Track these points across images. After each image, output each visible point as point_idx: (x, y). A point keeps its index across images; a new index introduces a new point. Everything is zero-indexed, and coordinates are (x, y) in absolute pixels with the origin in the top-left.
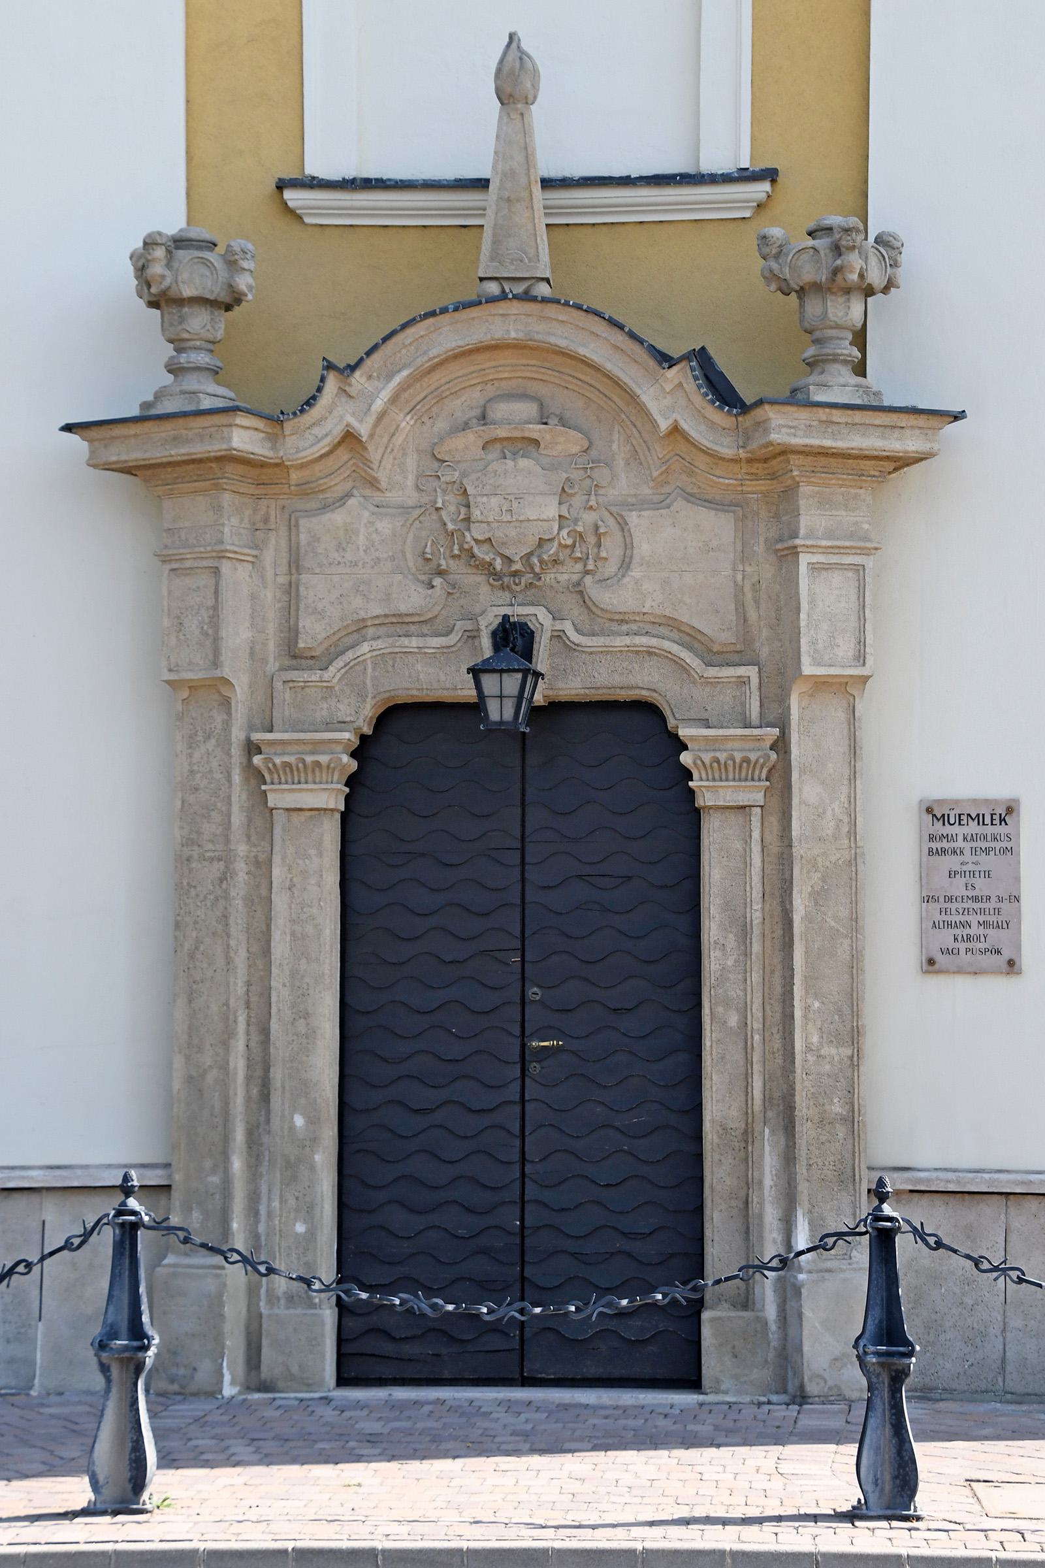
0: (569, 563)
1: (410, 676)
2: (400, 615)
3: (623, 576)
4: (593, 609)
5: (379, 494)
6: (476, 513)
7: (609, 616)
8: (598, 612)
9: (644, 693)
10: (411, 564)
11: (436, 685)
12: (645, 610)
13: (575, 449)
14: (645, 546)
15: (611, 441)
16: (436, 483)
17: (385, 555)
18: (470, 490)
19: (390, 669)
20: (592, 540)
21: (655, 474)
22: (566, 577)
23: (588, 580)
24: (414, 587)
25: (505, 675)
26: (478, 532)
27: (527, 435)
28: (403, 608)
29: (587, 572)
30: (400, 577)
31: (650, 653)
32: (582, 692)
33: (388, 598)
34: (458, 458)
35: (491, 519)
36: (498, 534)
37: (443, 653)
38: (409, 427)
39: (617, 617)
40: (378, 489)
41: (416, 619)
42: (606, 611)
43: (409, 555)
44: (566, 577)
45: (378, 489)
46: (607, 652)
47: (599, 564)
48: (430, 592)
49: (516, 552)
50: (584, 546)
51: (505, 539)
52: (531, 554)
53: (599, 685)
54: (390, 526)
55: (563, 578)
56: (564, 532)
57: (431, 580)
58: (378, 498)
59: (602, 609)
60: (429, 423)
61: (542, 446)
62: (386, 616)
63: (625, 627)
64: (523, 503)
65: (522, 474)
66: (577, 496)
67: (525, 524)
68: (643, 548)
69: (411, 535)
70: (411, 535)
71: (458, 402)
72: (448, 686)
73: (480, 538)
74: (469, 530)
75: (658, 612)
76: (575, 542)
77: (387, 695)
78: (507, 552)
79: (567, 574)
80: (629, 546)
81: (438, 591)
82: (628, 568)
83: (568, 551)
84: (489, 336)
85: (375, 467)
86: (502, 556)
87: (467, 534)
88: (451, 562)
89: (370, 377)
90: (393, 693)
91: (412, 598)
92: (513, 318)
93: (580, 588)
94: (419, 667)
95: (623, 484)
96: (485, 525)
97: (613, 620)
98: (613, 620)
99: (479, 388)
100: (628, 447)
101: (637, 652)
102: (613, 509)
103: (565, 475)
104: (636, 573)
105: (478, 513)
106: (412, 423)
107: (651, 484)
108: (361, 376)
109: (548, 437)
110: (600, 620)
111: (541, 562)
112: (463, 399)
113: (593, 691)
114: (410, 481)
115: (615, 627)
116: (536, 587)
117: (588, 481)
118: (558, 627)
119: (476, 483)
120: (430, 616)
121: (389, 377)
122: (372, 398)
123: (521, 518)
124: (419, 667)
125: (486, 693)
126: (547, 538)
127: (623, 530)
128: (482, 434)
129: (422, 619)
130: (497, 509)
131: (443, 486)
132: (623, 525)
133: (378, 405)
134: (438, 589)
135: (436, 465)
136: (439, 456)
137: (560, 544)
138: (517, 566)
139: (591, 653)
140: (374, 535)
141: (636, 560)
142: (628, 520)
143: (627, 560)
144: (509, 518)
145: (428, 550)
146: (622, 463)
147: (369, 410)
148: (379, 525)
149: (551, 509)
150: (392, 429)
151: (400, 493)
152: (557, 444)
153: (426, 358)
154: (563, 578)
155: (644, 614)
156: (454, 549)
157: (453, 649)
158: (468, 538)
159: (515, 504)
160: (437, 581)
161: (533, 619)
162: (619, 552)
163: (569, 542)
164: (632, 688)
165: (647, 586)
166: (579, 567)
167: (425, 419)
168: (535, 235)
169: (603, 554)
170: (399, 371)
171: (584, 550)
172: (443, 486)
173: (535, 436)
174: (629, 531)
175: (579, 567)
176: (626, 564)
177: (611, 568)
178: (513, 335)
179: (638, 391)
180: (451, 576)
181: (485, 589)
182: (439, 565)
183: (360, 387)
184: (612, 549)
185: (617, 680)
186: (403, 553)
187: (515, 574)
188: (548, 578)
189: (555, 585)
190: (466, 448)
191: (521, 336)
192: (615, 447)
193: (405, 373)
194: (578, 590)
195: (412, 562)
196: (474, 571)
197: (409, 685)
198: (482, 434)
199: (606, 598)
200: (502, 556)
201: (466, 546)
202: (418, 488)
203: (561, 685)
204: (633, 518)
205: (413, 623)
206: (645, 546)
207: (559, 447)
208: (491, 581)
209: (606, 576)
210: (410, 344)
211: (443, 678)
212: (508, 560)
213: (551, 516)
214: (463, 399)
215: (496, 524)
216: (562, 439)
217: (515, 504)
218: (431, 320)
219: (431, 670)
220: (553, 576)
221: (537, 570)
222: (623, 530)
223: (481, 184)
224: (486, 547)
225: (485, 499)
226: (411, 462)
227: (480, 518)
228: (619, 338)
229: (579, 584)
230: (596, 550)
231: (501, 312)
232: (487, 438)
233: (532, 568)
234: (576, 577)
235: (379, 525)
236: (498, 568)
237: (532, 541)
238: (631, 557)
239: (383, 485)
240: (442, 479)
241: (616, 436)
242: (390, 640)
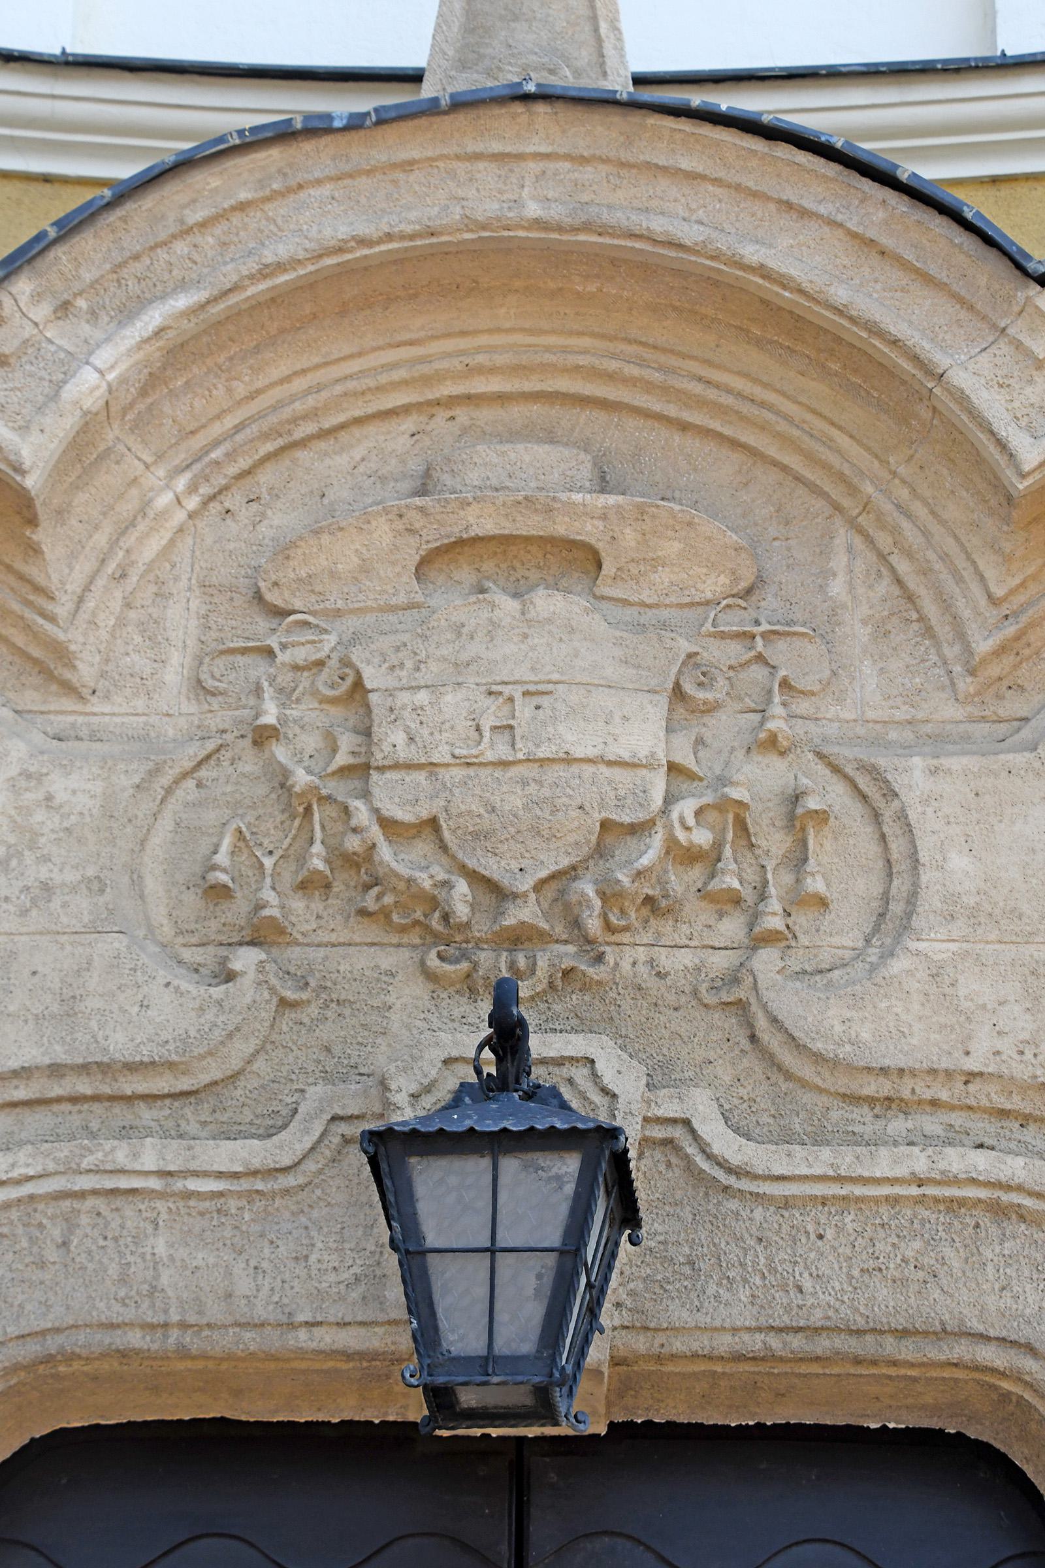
0: (699, 914)
1: (123, 1280)
2: (105, 1068)
3: (889, 954)
4: (787, 1058)
5: (68, 704)
6: (393, 741)
7: (842, 1083)
8: (807, 1071)
9: (988, 1355)
10: (159, 913)
11: (215, 1312)
12: (972, 1064)
13: (713, 585)
14: (959, 862)
15: (828, 573)
16: (259, 669)
17: (71, 876)
18: (372, 677)
19: (52, 1255)
20: (774, 842)
21: (983, 646)
22: (686, 958)
23: (766, 961)
24: (162, 975)
25: (510, 1165)
26: (395, 797)
27: (561, 528)
28: (119, 1044)
29: (760, 940)
30: (119, 943)
31: (998, 1210)
32: (755, 1343)
33: (70, 1008)
34: (335, 601)
35: (441, 754)
36: (465, 800)
37: (252, 1195)
38: (180, 516)
39: (872, 1087)
40: (69, 689)
41: (162, 1084)
42: (834, 1064)
43: (153, 885)
44: (686, 958)
45: (69, 689)
46: (843, 1198)
47: (802, 920)
48: (218, 992)
49: (522, 866)
50: (744, 862)
51: (487, 821)
52: (570, 873)
53: (817, 1318)
54: (98, 787)
55: (678, 961)
56: (686, 808)
57: (224, 961)
58: (65, 713)
59: (818, 1058)
60: (245, 513)
61: (608, 568)
62: (56, 1070)
63: (898, 1125)
64: (555, 719)
65: (551, 633)
66: (722, 716)
67: (558, 772)
68: (953, 866)
69: (166, 823)
70: (166, 823)
71: (342, 461)
72: (261, 1311)
73: (400, 814)
74: (366, 795)
75: (1022, 1072)
76: (718, 846)
77: (33, 1349)
78: (491, 868)
79: (697, 946)
80: (901, 866)
81: (245, 991)
82: (905, 925)
83: (696, 874)
84: (457, 212)
85: (61, 611)
86: (476, 878)
87: (358, 804)
88: (298, 904)
89: (64, 309)
90: (53, 1344)
91: (153, 1010)
92: (533, 166)
93: (741, 993)
94: (160, 1246)
95: (866, 687)
96: (421, 777)
97: (854, 1099)
98: (854, 1099)
99: (409, 424)
100: (884, 587)
101: (954, 1205)
102: (845, 754)
103: (685, 646)
104: (934, 942)
105: (399, 738)
106: (192, 503)
107: (966, 685)
108: (37, 298)
109: (629, 537)
110: (808, 1098)
111: (610, 896)
112: (358, 453)
113: (797, 1342)
114: (175, 673)
115: (863, 1120)
116: (587, 986)
117: (758, 672)
118: (670, 1109)
119: (394, 659)
120: (214, 1071)
121: (127, 313)
122: (69, 364)
123: (543, 752)
124: (160, 1246)
125: (432, 1239)
126: (627, 819)
127: (877, 817)
128: (418, 522)
129: (184, 1084)
130: (463, 726)
131: (285, 678)
132: (876, 796)
133: (87, 386)
134: (246, 983)
135: (262, 624)
136: (271, 597)
137: (672, 847)
138: (524, 913)
139: (787, 1203)
140: (39, 816)
141: (931, 900)
142: (898, 782)
143: (897, 908)
144: (502, 751)
145: (222, 858)
146: (863, 633)
147: (55, 396)
148: (59, 785)
149: (643, 732)
150: (126, 508)
151: (140, 704)
152: (656, 563)
153: (252, 266)
154: (678, 961)
155: (971, 1077)
156: (319, 853)
157: (290, 1181)
158: (362, 814)
159: (524, 711)
160: (246, 960)
161: (580, 1074)
162: (867, 886)
163: (702, 838)
164: (944, 1334)
165: (972, 986)
166: (732, 928)
167: (234, 500)
168: (594, 19)
169: (816, 885)
170: (164, 297)
171: (751, 875)
172: (285, 678)
173: (590, 531)
174: (902, 816)
175: (732, 928)
176: (892, 920)
177: (842, 932)
178: (533, 210)
179: (941, 360)
180: (295, 953)
181: (410, 993)
182: (260, 906)
183: (29, 331)
184: (842, 867)
185: (884, 1301)
186: (137, 880)
187: (518, 938)
188: (628, 959)
189: (652, 983)
190: (365, 569)
191: (556, 212)
192: (837, 588)
193: (182, 302)
194: (736, 1003)
195: (161, 898)
196: (373, 932)
197: (117, 1313)
198: (418, 522)
199: (831, 1021)
200: (476, 878)
201: (353, 843)
202: (200, 689)
203: (680, 1314)
204: (914, 778)
205: (150, 1098)
206: (959, 862)
207: (663, 577)
208: (433, 961)
209: (825, 958)
210: (203, 225)
211: (244, 1285)
212: (494, 891)
213: (643, 753)
214: (358, 453)
215: (458, 773)
216: (672, 548)
217: (524, 711)
218: (274, 155)
219: (201, 1257)
220: (642, 953)
221: (593, 925)
222: (877, 817)
223: (414, 77)
224: (423, 848)
225: (422, 697)
226: (182, 619)
227: (404, 753)
228: (878, 210)
229: (734, 980)
230: (788, 878)
231: (496, 147)
232: (433, 536)
233: (576, 924)
234: (720, 962)
235: (59, 785)
236: (462, 911)
237: (578, 831)
238: (912, 898)
239: (86, 672)
240: (282, 657)
241: (840, 561)
242: (64, 1150)
